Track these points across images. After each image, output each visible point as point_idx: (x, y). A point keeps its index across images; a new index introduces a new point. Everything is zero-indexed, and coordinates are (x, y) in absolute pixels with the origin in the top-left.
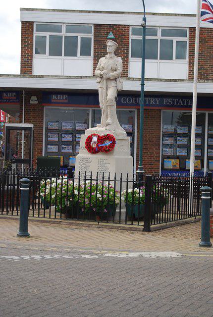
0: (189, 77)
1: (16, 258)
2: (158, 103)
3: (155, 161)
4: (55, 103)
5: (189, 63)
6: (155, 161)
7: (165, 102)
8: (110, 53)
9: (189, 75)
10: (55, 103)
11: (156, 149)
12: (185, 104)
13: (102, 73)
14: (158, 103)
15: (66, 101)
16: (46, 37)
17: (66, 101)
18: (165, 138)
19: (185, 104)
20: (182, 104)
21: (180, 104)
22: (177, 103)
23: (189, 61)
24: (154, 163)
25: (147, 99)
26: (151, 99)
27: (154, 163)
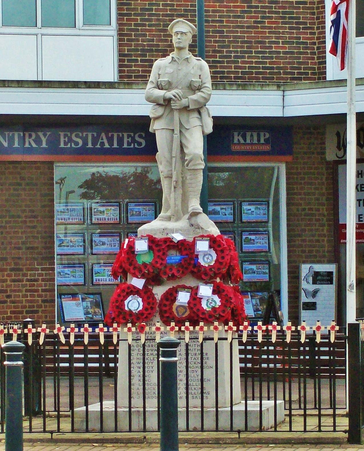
0: (120, 71)
1: (277, 357)
2: (44, 145)
3: (43, 301)
4: (238, 153)
5: (119, 35)
6: (43, 301)
7: (62, 140)
8: (180, 49)
9: (120, 66)
10: (238, 153)
11: (43, 269)
12: (115, 146)
13: (169, 94)
14: (44, 145)
15: (268, 148)
16: (315, 67)
17: (268, 148)
18: (265, 220)
19: (115, 146)
20: (107, 146)
21: (103, 144)
22: (95, 141)
23: (120, 30)
24: (41, 306)
25: (115, 135)
26: (27, 134)
27: (41, 306)
